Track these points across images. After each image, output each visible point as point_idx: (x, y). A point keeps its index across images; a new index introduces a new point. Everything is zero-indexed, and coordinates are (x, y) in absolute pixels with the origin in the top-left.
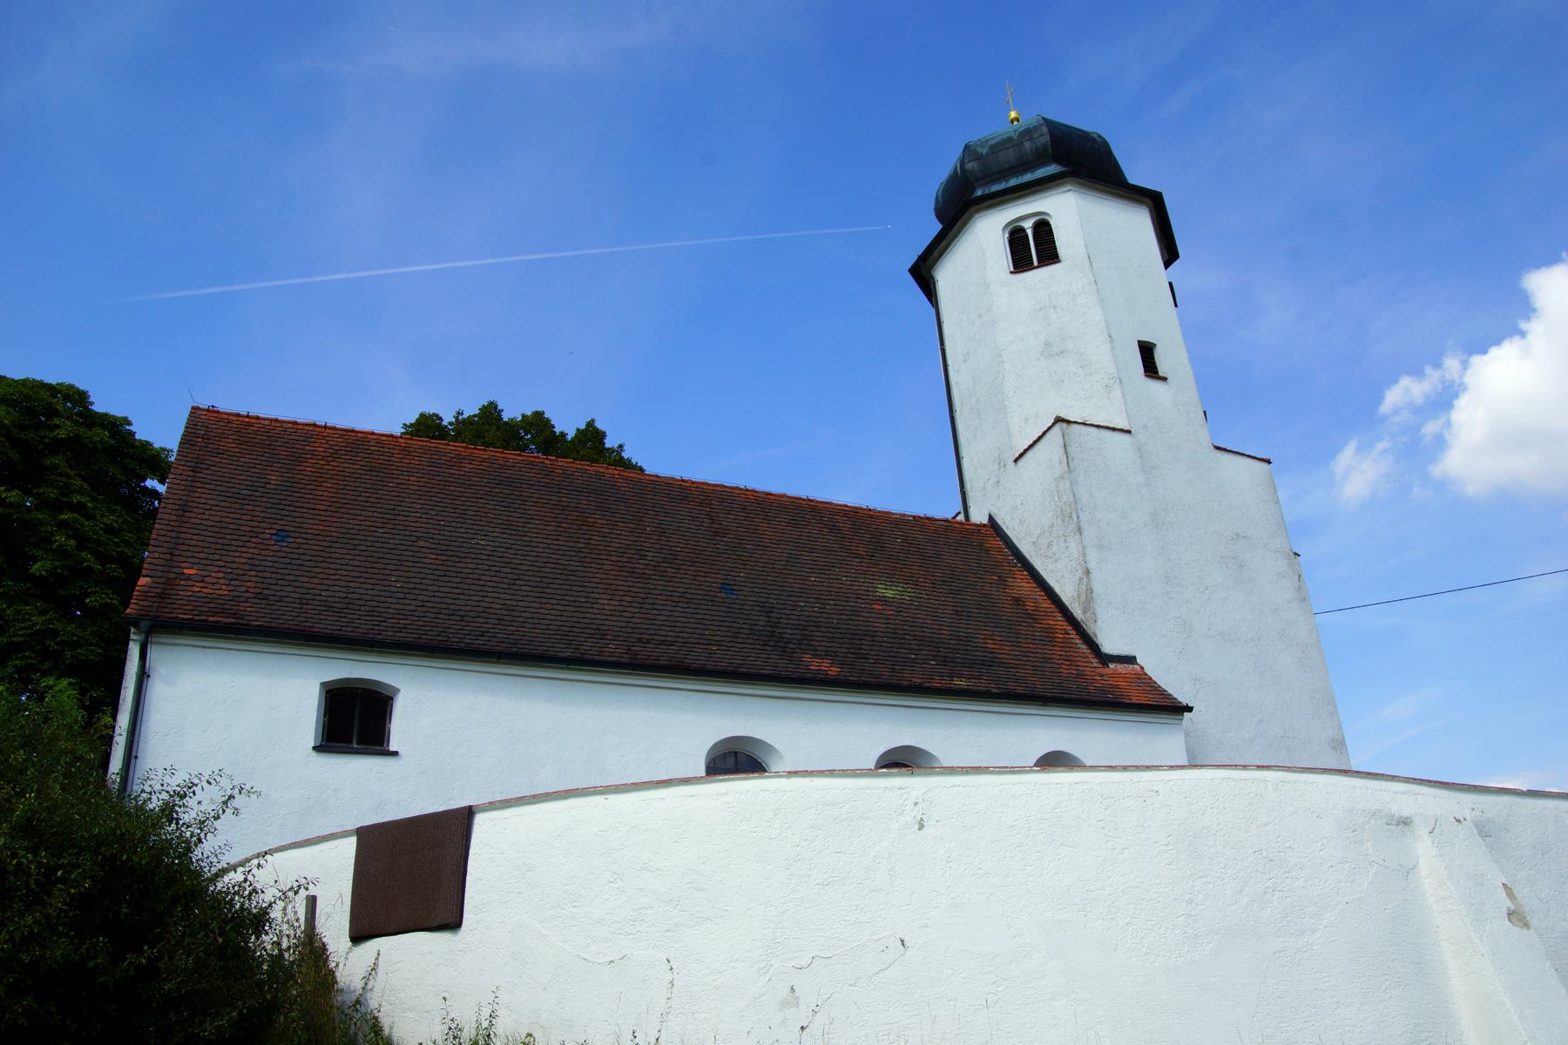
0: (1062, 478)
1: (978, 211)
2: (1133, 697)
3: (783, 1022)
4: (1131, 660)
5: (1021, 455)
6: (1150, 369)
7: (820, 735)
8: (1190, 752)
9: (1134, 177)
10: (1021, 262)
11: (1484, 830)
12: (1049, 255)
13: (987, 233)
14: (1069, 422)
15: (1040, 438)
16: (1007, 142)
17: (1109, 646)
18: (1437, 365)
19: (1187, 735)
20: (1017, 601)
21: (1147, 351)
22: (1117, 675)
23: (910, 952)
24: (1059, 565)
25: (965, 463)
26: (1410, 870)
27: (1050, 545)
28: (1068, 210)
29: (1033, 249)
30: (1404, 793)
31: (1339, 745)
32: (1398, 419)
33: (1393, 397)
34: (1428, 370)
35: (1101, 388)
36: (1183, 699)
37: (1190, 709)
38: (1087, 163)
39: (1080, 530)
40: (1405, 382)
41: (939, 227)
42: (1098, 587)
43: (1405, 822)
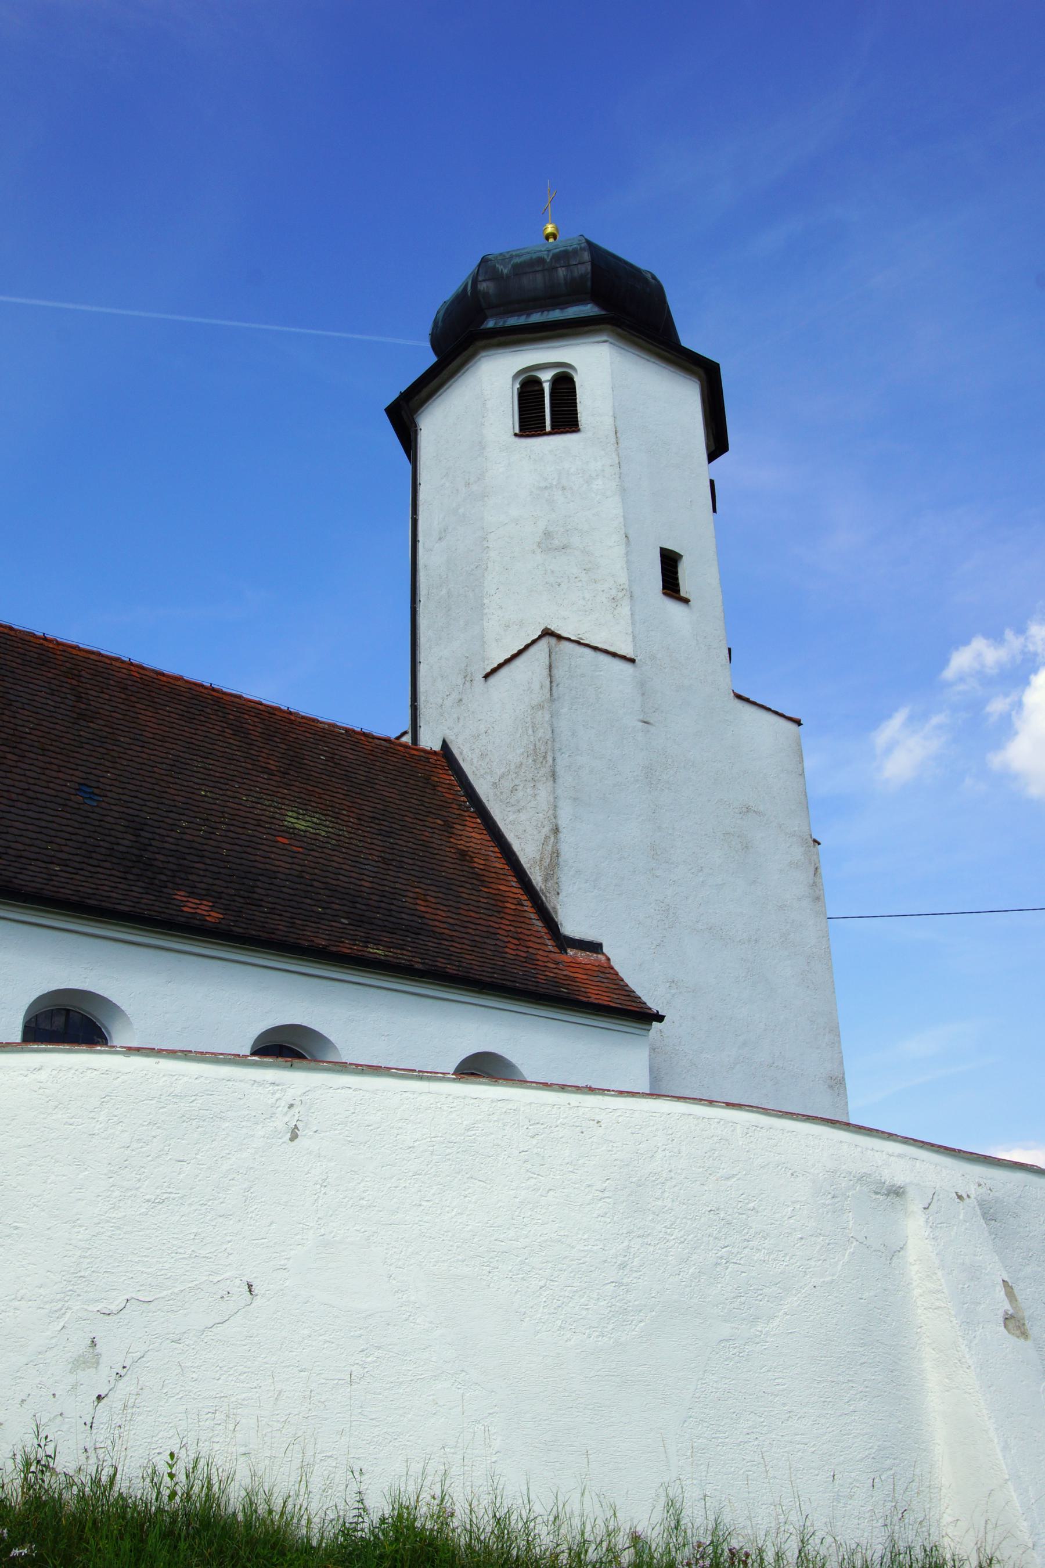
0: (541, 707)
1: (486, 347)
2: (593, 995)
3: (74, 1387)
4: (595, 947)
5: (494, 671)
6: (671, 586)
7: (185, 999)
8: (655, 1076)
9: (688, 340)
10: (530, 424)
11: (990, 1212)
12: (567, 421)
13: (492, 381)
14: (559, 637)
15: (520, 652)
16: (536, 264)
17: (572, 926)
18: (1021, 630)
19: (653, 1049)
20: (463, 855)
21: (670, 561)
22: (575, 964)
23: (258, 1301)
24: (523, 816)
25: (422, 670)
26: (894, 1253)
27: (514, 789)
28: (598, 366)
29: (548, 409)
30: (899, 1156)
31: (837, 1083)
32: (961, 687)
33: (962, 660)
34: (1009, 634)
35: (610, 600)
36: (654, 1004)
37: (660, 1018)
38: (633, 310)
39: (554, 776)
40: (979, 644)
41: (433, 359)
42: (567, 850)
43: (897, 1192)
